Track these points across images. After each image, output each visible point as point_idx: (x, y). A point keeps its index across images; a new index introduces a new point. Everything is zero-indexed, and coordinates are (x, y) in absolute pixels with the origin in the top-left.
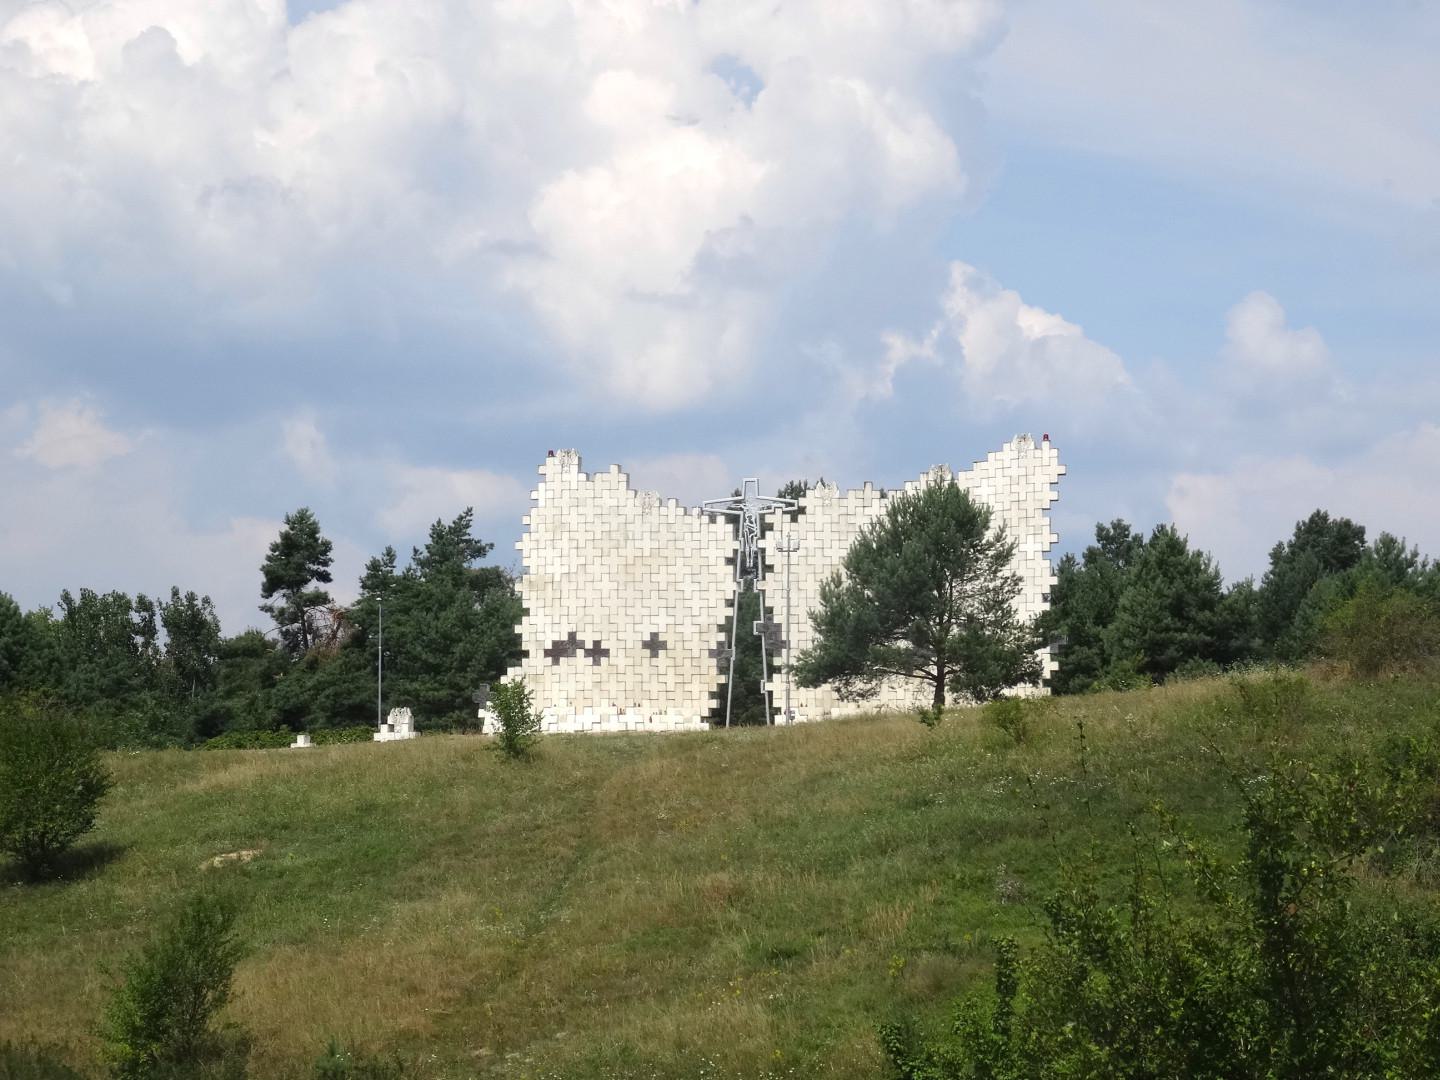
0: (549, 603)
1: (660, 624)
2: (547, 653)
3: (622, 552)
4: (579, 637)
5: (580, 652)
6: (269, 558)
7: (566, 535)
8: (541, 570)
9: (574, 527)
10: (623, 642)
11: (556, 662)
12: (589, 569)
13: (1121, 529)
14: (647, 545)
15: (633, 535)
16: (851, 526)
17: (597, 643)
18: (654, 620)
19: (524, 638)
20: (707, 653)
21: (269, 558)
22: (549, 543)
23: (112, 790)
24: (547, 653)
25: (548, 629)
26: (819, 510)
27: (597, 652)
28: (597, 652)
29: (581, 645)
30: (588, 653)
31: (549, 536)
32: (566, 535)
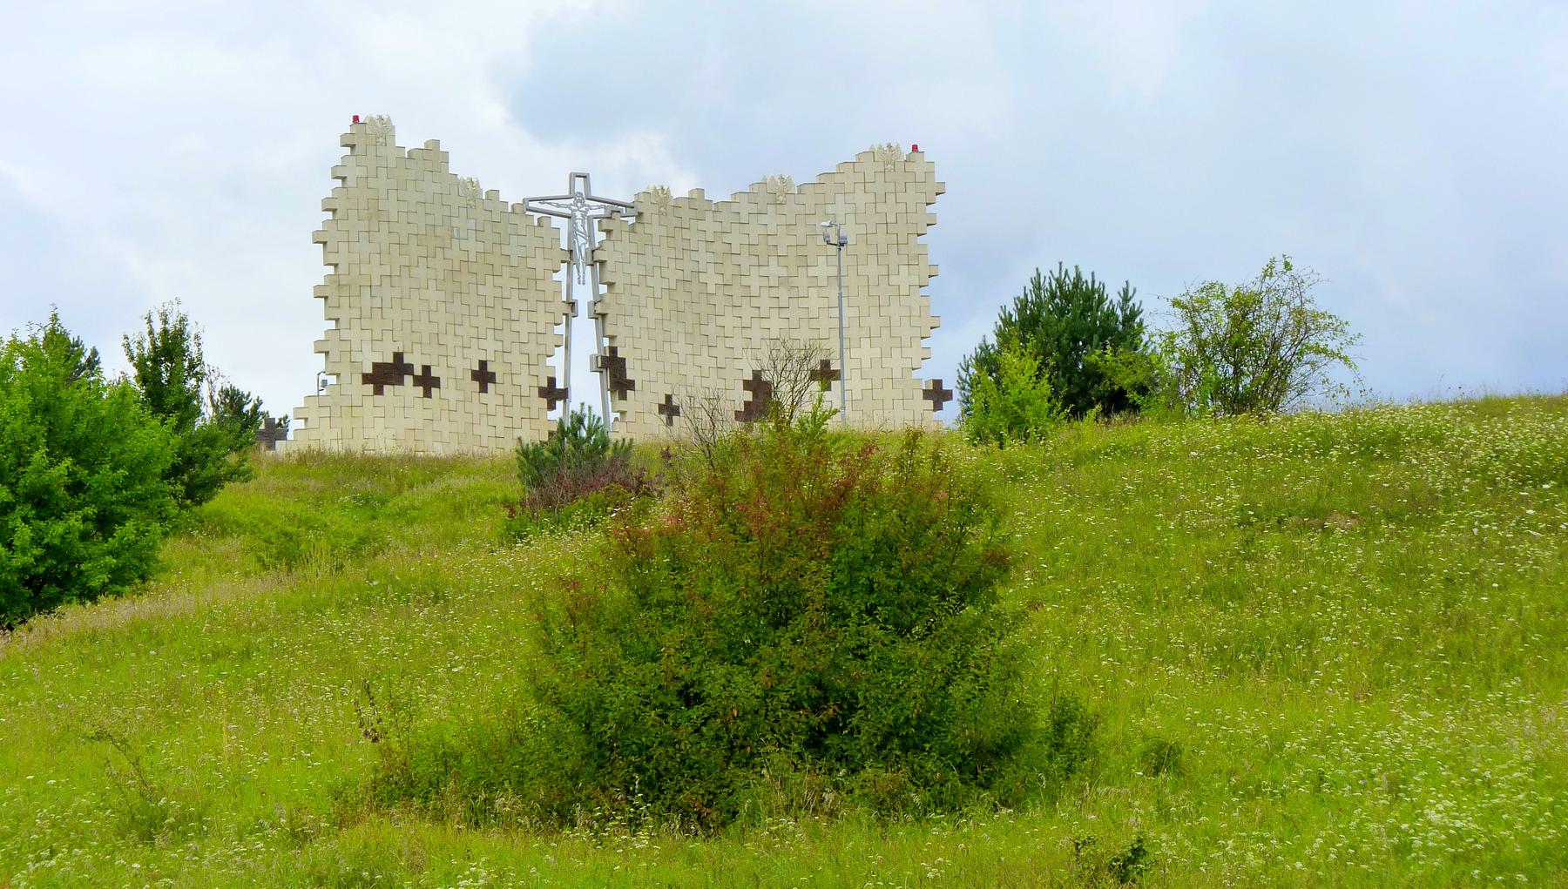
0: (366, 313)
1: (488, 350)
2: (367, 379)
3: (448, 254)
4: (407, 360)
5: (408, 379)
6: (880, 147)
7: (384, 226)
8: (355, 270)
9: (394, 217)
10: (454, 371)
11: (379, 391)
12: (414, 271)
13: (317, 288)
14: (473, 247)
15: (458, 233)
16: (686, 242)
17: (426, 369)
18: (483, 344)
19: (379, 360)
20: (537, 390)
21: (880, 147)
22: (363, 235)
23: (163, 576)
24: (367, 379)
25: (367, 347)
26: (655, 217)
27: (428, 382)
28: (428, 382)
29: (409, 369)
30: (418, 381)
31: (364, 225)
32: (384, 226)
